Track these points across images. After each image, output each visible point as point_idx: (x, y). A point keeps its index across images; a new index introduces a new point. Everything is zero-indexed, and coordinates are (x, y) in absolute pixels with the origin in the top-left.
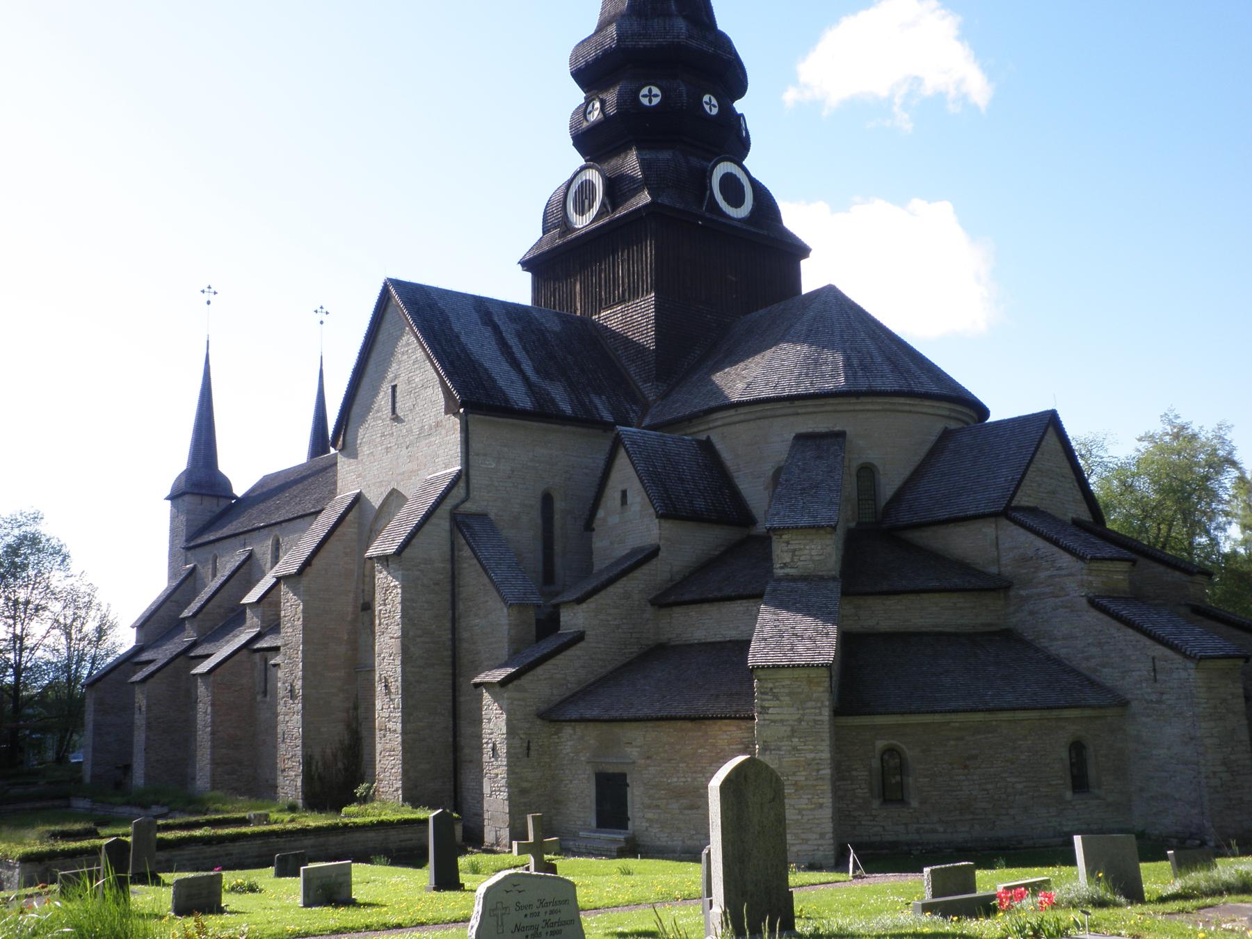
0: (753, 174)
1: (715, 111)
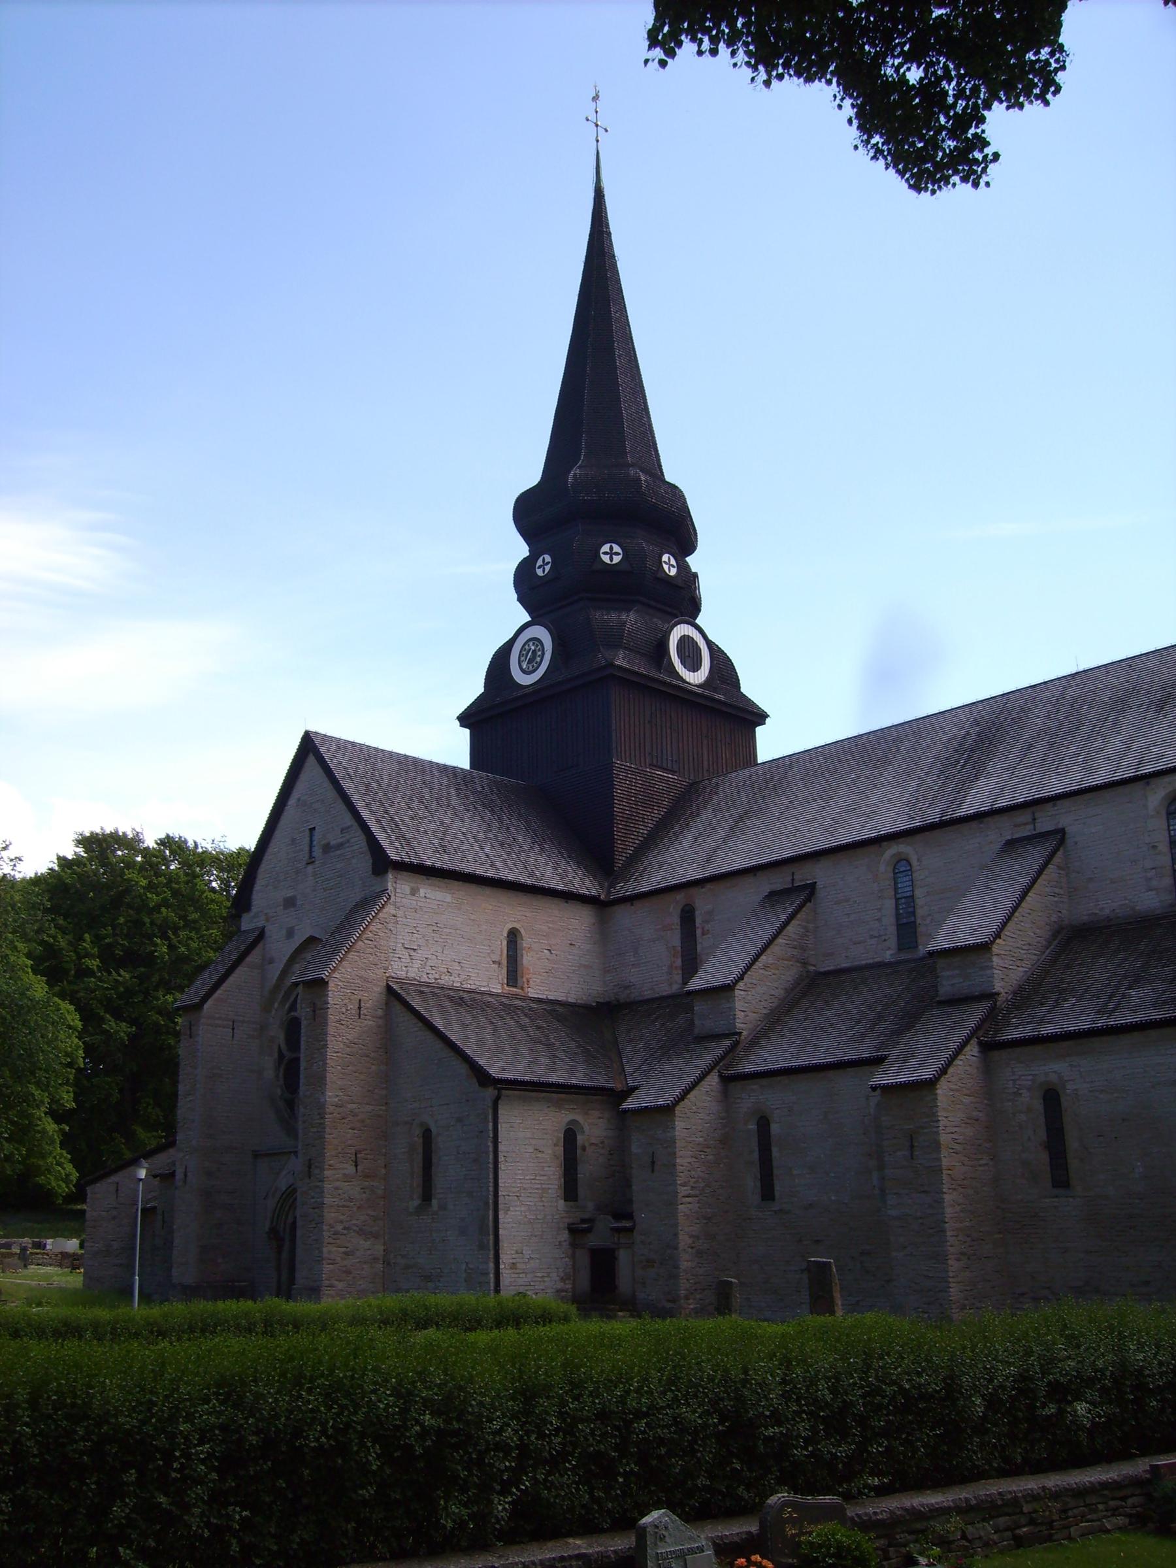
0: (710, 637)
1: (673, 572)
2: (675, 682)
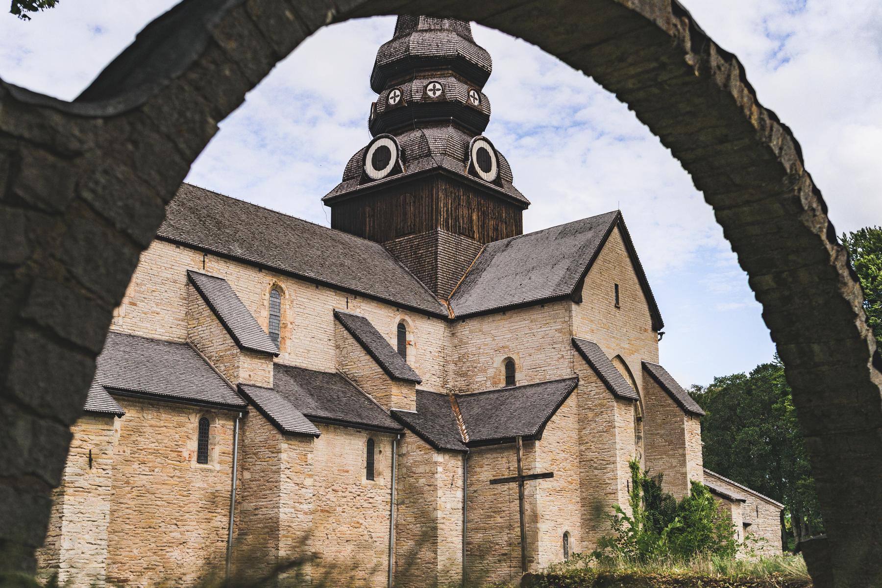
0: (496, 147)
2: (477, 179)
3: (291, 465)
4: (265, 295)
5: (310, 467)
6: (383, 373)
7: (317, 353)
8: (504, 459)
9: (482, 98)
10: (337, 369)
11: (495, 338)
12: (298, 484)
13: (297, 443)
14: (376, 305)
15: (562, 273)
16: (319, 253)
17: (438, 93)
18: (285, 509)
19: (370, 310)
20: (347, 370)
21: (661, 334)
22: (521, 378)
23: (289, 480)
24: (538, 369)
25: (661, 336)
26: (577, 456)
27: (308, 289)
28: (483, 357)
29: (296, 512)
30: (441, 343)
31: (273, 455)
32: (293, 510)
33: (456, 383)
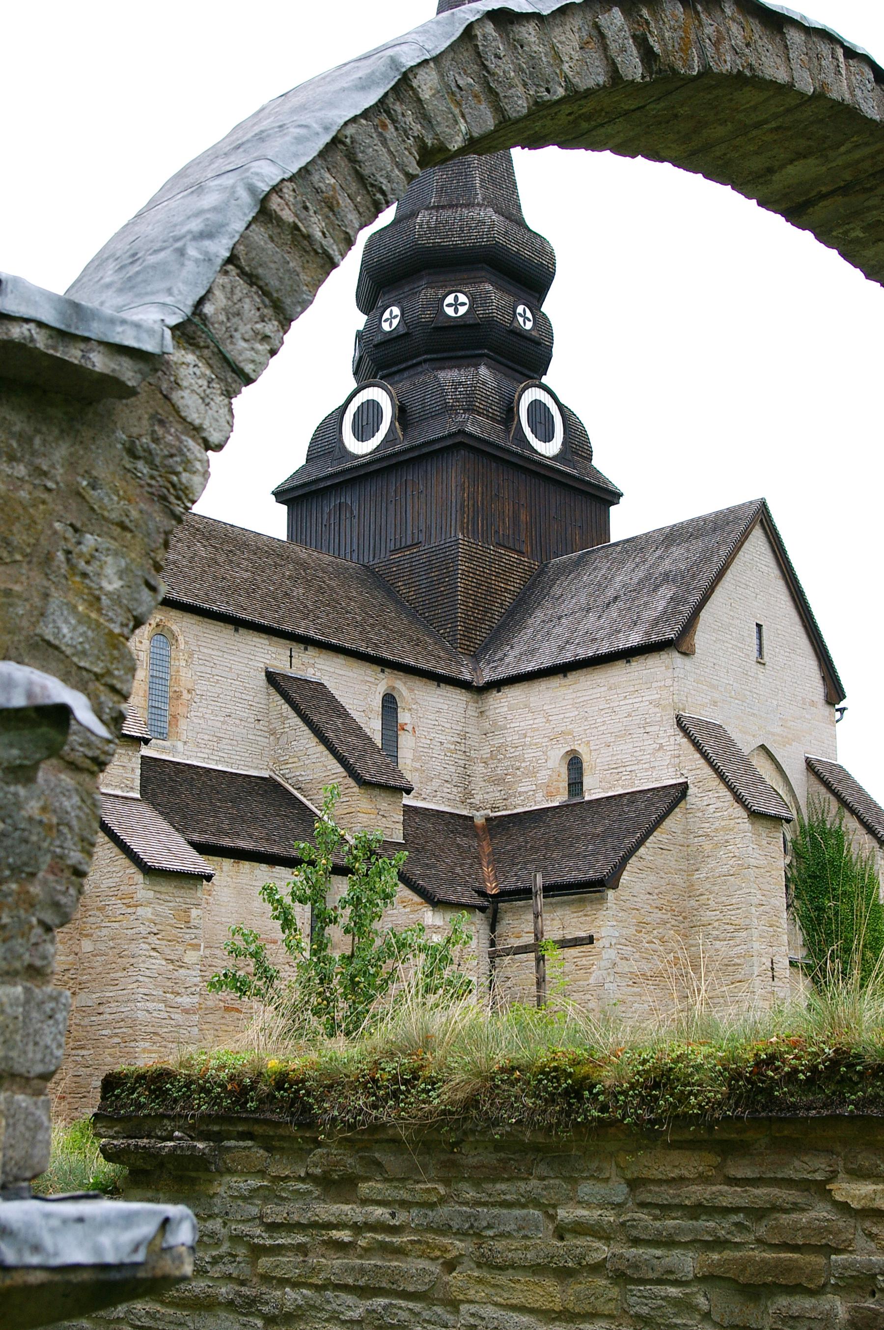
0: (562, 400)
1: (529, 326)
2: (527, 453)
3: (160, 927)
4: (141, 642)
5: (195, 931)
6: (345, 774)
7: (235, 743)
8: (555, 922)
9: (543, 323)
10: (271, 770)
11: (550, 718)
12: (172, 961)
13: (171, 889)
14: (344, 662)
15: (661, 605)
16: (246, 575)
17: (462, 310)
18: (148, 1004)
19: (332, 670)
20: (287, 771)
21: (842, 710)
22: (593, 790)
23: (154, 954)
24: (619, 770)
25: (842, 714)
26: (685, 918)
27: (218, 634)
28: (530, 751)
29: (169, 1009)
30: (461, 728)
31: (130, 910)
32: (162, 1006)
33: (486, 796)
